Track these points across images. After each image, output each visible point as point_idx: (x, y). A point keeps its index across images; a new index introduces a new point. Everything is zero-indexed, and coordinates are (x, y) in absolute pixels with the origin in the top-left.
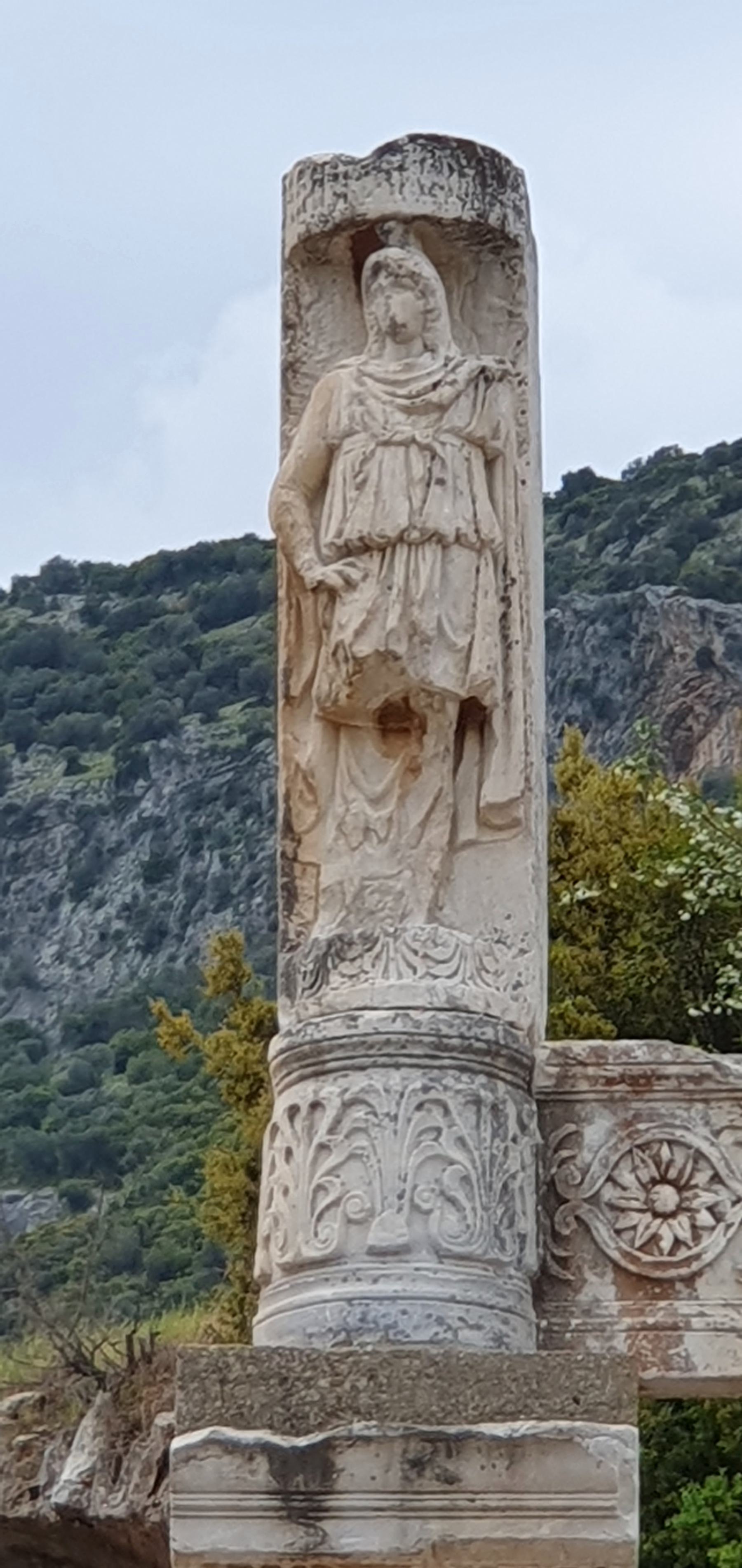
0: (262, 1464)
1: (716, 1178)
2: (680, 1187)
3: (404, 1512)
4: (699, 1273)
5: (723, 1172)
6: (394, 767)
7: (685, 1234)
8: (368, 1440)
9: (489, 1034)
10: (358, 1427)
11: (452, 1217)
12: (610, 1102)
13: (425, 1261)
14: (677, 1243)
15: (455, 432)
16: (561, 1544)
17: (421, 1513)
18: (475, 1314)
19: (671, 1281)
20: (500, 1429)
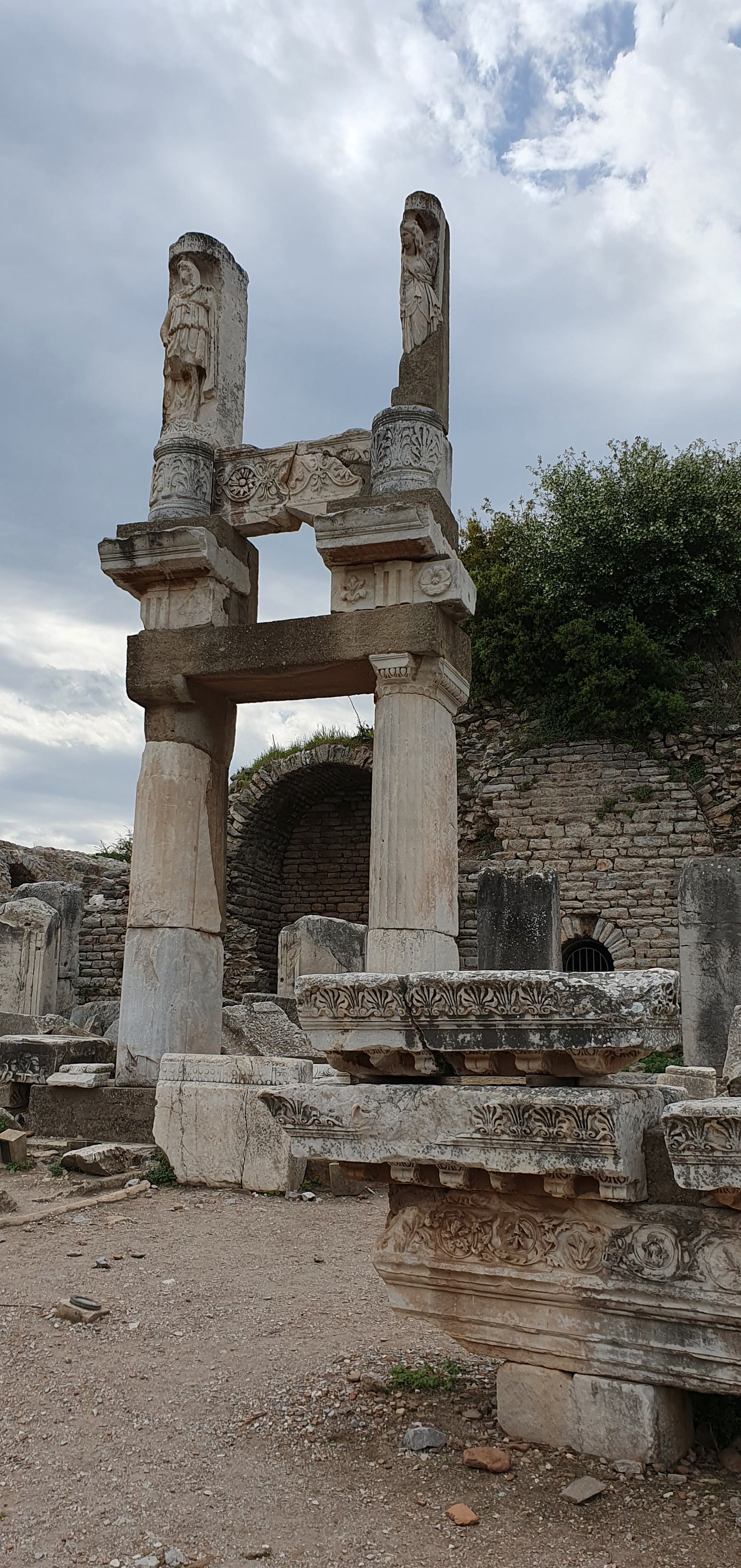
0: (118, 545)
1: (254, 476)
2: (247, 479)
3: (152, 554)
4: (249, 500)
6: (187, 387)
7: (246, 490)
8: (139, 536)
9: (195, 443)
10: (136, 533)
11: (181, 487)
12: (232, 461)
13: (175, 499)
14: (245, 492)
15: (193, 301)
16: (189, 559)
17: (155, 554)
18: (186, 511)
19: (243, 502)
20: (169, 530)
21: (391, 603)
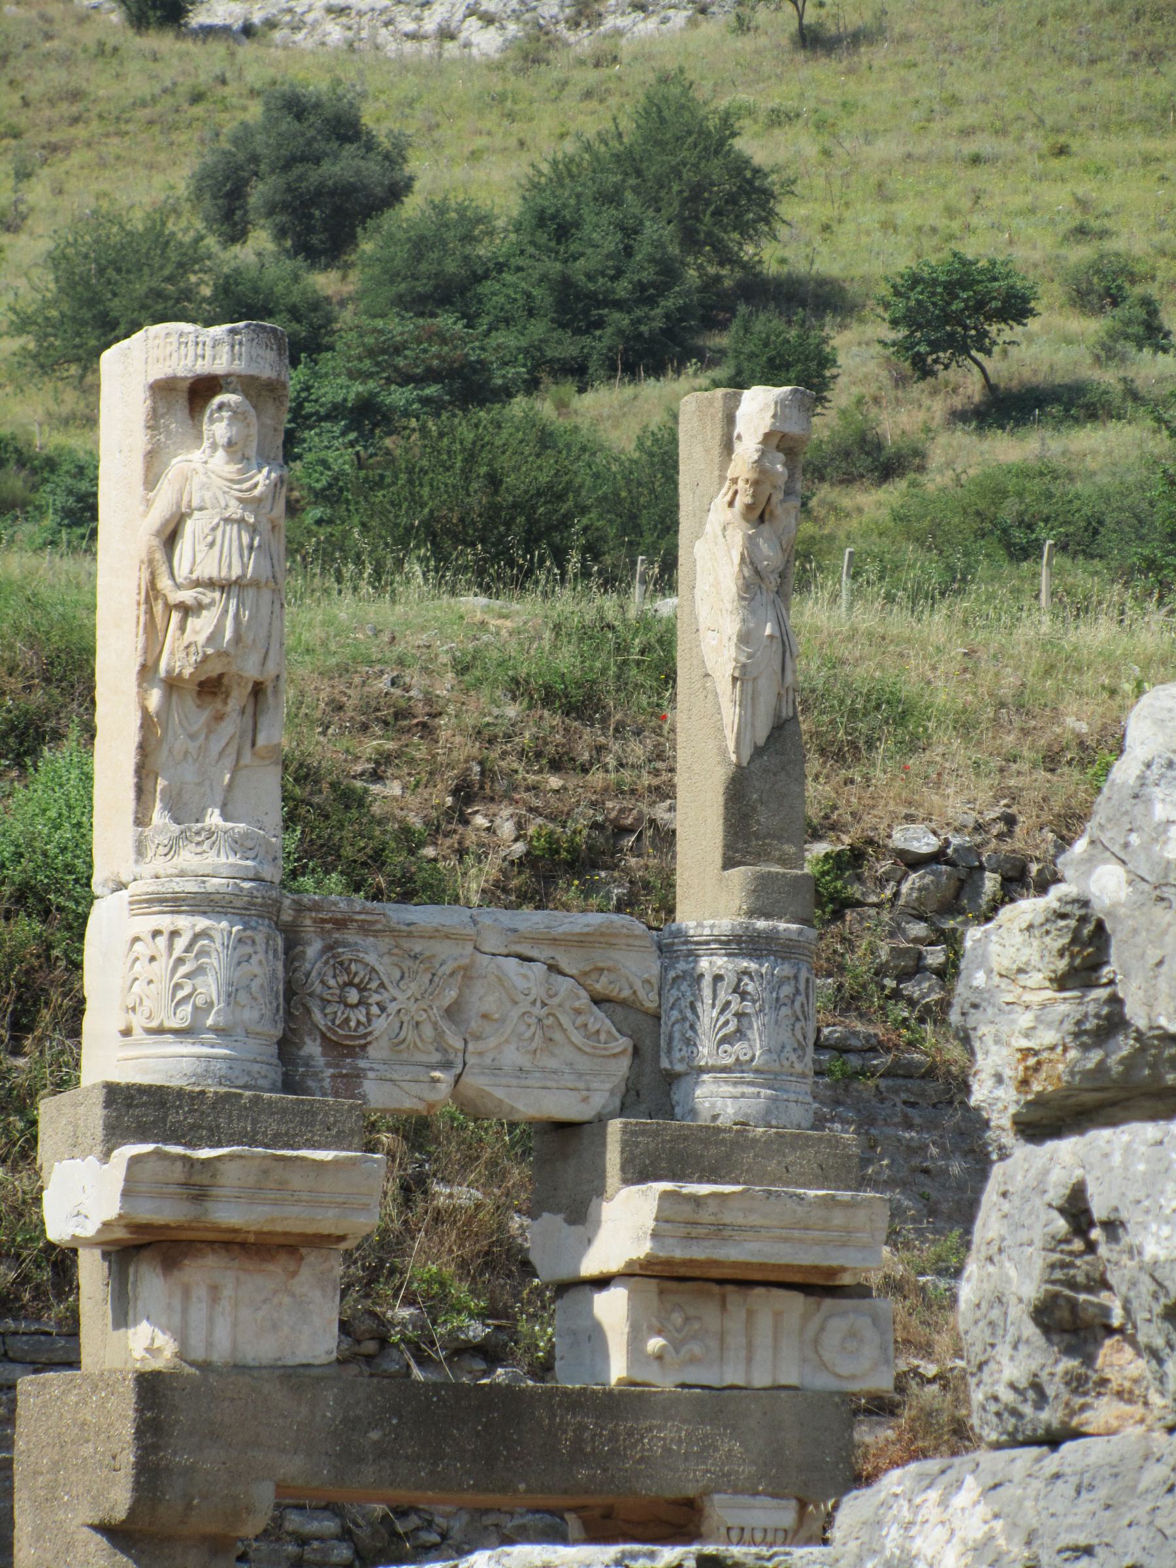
5: (386, 981)
21: (761, 1379)
